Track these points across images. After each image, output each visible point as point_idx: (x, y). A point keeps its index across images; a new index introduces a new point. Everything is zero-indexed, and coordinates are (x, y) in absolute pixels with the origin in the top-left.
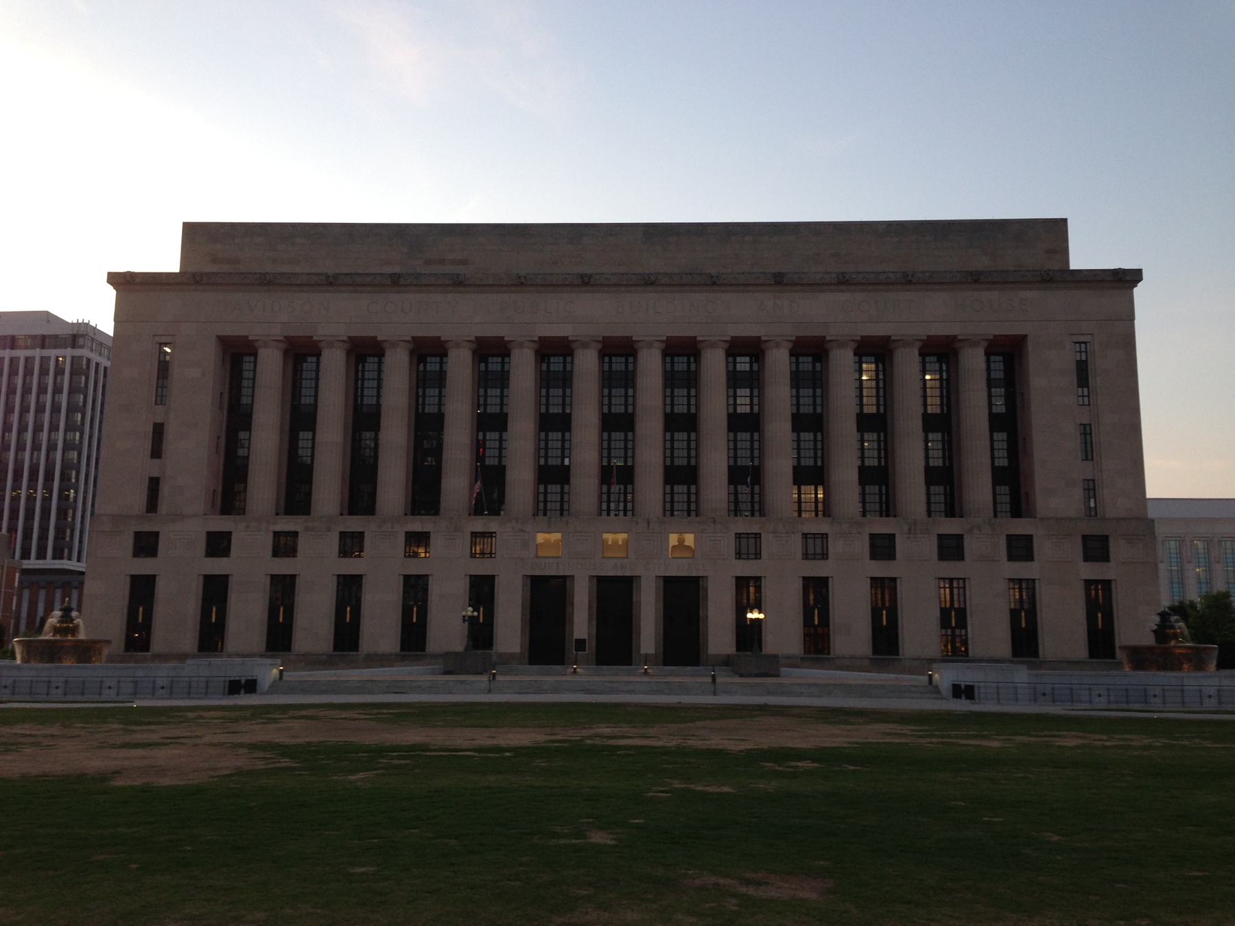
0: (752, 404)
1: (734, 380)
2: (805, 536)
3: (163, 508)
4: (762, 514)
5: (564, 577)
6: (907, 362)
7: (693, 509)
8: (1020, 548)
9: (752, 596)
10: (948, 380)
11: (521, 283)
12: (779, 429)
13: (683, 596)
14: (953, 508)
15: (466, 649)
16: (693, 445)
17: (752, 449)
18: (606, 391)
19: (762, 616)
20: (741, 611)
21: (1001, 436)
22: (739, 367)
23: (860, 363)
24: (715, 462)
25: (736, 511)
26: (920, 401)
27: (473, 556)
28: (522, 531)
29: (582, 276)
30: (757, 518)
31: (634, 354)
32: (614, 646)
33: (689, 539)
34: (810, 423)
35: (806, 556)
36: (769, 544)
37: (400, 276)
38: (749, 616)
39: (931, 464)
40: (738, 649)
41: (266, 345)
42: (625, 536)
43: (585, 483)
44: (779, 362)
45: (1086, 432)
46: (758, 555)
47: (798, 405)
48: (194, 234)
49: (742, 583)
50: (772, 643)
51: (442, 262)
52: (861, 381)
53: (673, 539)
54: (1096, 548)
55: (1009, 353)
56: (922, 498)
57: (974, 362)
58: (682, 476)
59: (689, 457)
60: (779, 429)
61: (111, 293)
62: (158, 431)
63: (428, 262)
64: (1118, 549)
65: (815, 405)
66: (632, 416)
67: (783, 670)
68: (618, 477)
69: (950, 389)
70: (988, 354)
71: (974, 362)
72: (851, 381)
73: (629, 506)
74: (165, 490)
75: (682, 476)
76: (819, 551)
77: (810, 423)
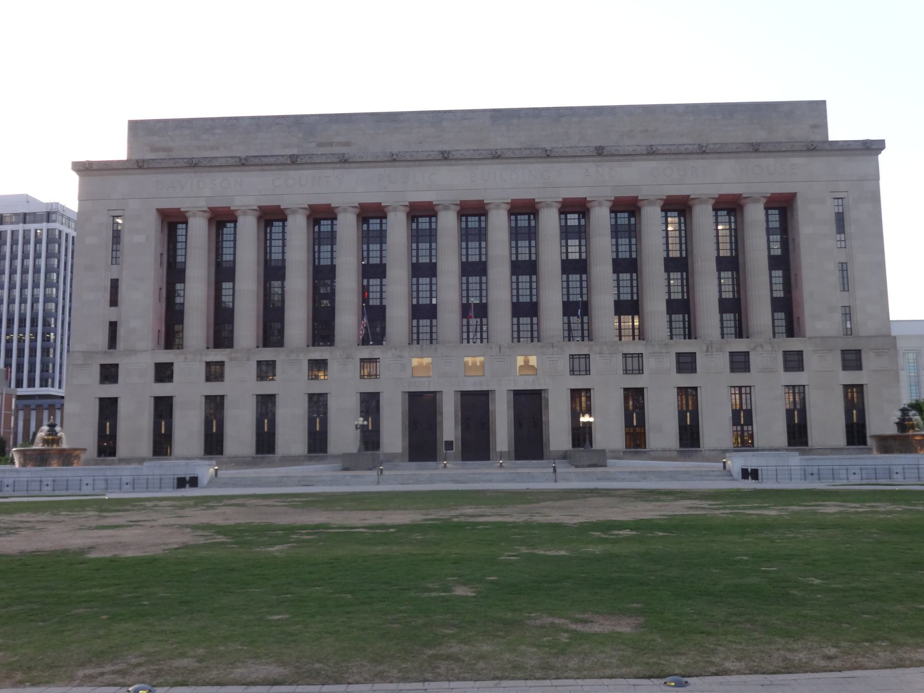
0: (580, 252)
1: (515, 234)
2: (625, 356)
3: (121, 344)
4: (590, 339)
5: (435, 393)
6: (703, 216)
7: (535, 336)
8: (794, 361)
9: (584, 405)
10: (736, 230)
11: (393, 159)
13: (529, 405)
14: (740, 332)
15: (359, 450)
16: (534, 285)
17: (581, 287)
19: (591, 420)
20: (575, 416)
21: (778, 273)
22: (569, 223)
23: (666, 217)
24: (552, 299)
26: (715, 246)
27: (362, 377)
28: (400, 357)
29: (442, 153)
32: (476, 445)
33: (533, 360)
34: (627, 266)
35: (626, 371)
36: (596, 363)
39: (723, 297)
40: (574, 446)
41: (194, 215)
42: (482, 359)
44: (601, 217)
45: (844, 268)
46: (588, 372)
48: (137, 128)
49: (575, 393)
50: (600, 440)
51: (331, 144)
53: (520, 361)
54: (852, 360)
55: (783, 207)
56: (665, 325)
57: (755, 215)
58: (526, 309)
59: (531, 295)
63: (320, 145)
64: (868, 360)
68: (475, 312)
69: (737, 237)
70: (767, 208)
71: (755, 215)
72: (657, 233)
73: (485, 335)
74: (121, 332)
75: (526, 309)
76: (636, 367)
77: (627, 266)
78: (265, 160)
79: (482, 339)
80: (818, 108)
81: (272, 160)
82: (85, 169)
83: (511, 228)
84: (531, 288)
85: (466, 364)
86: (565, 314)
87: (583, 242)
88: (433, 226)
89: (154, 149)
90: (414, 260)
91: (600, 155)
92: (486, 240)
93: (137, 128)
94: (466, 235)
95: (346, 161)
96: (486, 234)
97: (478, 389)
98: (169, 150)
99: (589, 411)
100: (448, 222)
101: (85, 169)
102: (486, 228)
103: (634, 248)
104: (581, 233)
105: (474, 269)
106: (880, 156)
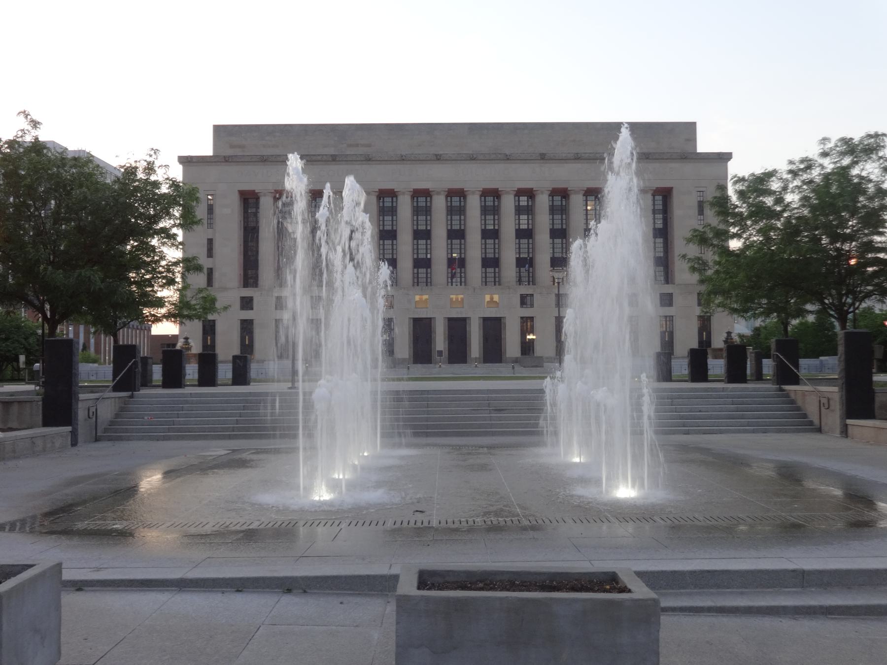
0: (528, 224)
1: (485, 211)
3: (216, 284)
4: (534, 284)
5: (430, 318)
11: (403, 159)
12: (543, 238)
13: (493, 328)
16: (497, 246)
18: (381, 218)
20: (523, 334)
22: (521, 203)
23: (587, 201)
24: (509, 256)
25: (520, 281)
29: (436, 155)
30: (531, 286)
31: (465, 197)
32: (458, 353)
33: (496, 298)
37: (336, 156)
38: (528, 337)
40: (522, 354)
41: (265, 195)
43: (440, 268)
44: (543, 202)
46: (532, 306)
47: (553, 224)
48: (221, 132)
49: (524, 320)
50: (539, 351)
51: (357, 145)
52: (587, 210)
58: (491, 263)
59: (495, 253)
60: (543, 238)
61: (180, 167)
62: (210, 242)
63: (350, 146)
65: (562, 224)
66: (463, 230)
67: (545, 364)
68: (457, 265)
70: (654, 195)
73: (463, 280)
74: (216, 275)
75: (491, 263)
78: (314, 158)
79: (461, 282)
80: (689, 129)
81: (319, 158)
82: (185, 161)
83: (447, 207)
84: (494, 248)
85: (451, 299)
86: (483, 266)
87: (530, 217)
88: (394, 204)
89: (232, 147)
90: (415, 227)
91: (543, 159)
92: (430, 215)
93: (221, 132)
94: (451, 211)
95: (370, 160)
96: (430, 211)
97: (460, 316)
98: (242, 147)
99: (532, 332)
100: (439, 204)
101: (185, 161)
102: (430, 207)
103: (564, 221)
104: (529, 210)
105: (457, 235)
106: (729, 163)
